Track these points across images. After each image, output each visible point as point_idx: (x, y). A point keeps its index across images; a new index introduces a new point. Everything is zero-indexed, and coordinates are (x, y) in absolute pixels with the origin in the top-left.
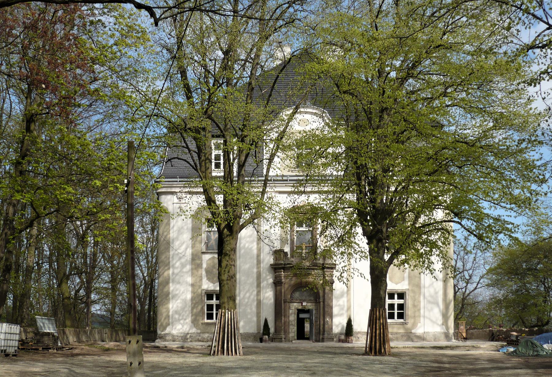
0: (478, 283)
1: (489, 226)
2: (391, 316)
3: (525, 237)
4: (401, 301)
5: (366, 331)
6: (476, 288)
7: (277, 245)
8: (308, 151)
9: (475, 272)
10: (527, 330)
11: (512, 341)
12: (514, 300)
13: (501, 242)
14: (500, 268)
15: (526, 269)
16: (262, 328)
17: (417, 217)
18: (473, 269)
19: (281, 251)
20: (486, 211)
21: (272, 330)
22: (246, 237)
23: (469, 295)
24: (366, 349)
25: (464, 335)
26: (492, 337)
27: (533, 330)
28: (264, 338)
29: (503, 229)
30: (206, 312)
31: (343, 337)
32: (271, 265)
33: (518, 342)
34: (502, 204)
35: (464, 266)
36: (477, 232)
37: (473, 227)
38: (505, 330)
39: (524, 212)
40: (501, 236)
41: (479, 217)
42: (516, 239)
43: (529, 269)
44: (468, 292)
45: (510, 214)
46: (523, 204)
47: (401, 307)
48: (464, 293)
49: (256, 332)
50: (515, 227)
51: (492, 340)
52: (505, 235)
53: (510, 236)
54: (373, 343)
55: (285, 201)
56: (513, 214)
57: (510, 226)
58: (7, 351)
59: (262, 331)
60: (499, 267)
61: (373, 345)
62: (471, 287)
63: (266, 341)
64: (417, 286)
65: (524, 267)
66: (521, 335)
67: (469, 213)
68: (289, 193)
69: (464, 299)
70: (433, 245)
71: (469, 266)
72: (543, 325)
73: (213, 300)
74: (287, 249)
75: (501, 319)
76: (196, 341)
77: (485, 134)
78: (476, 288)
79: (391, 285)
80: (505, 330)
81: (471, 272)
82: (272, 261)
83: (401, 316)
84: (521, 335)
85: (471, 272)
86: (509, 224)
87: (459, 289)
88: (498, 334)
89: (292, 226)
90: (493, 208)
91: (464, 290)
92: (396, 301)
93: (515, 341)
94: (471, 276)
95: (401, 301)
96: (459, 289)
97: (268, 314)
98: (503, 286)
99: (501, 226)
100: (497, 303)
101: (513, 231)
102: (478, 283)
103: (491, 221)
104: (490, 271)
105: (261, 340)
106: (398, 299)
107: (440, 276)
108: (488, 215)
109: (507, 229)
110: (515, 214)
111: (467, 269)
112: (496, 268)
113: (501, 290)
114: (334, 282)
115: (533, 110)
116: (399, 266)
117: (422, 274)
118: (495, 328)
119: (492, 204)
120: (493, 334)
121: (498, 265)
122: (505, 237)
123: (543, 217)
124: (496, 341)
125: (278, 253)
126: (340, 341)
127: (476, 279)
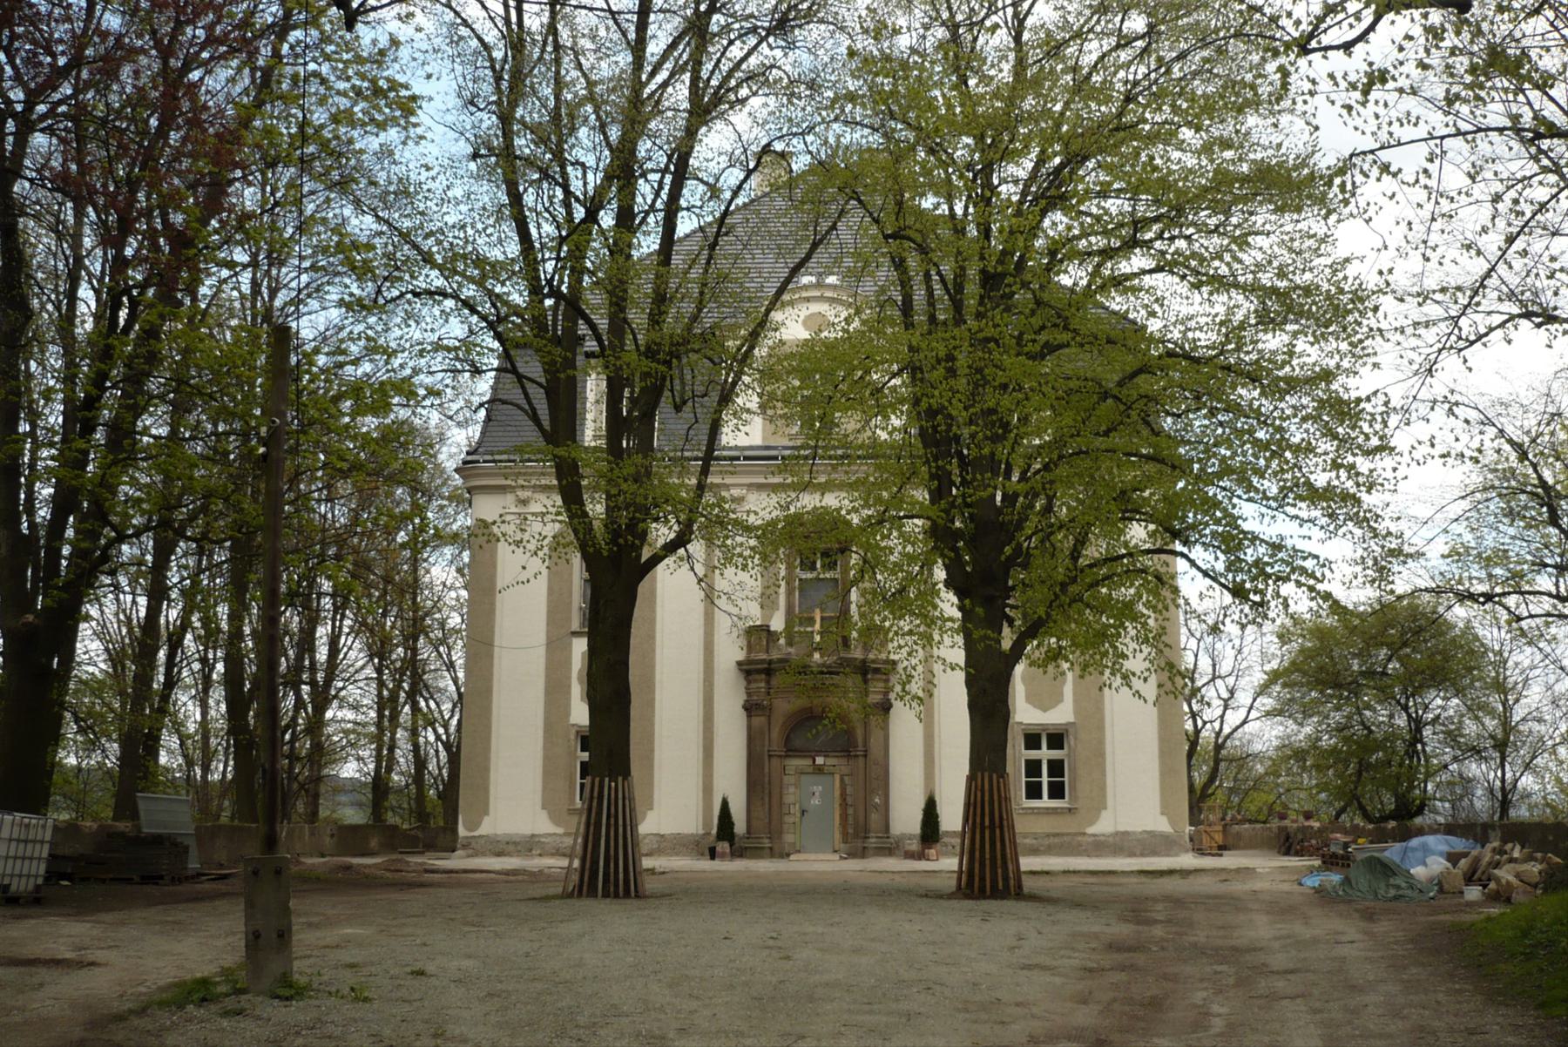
0: (1251, 708)
1: (1257, 563)
2: (1034, 791)
3: (1358, 595)
4: (1056, 754)
5: (960, 828)
6: (1245, 722)
7: (754, 613)
8: (822, 383)
9: (1243, 682)
10: (1371, 826)
11: (1334, 855)
12: (1334, 751)
13: (1290, 602)
14: (1298, 670)
15: (1362, 673)
16: (716, 821)
17: (1081, 542)
18: (1237, 672)
19: (765, 629)
20: (1246, 526)
21: (740, 827)
22: (672, 592)
23: (1228, 737)
24: (959, 879)
25: (1219, 838)
26: (1288, 844)
27: (1385, 829)
28: (719, 849)
29: (1293, 570)
30: (1066, 779)
31: (914, 846)
32: (739, 664)
33: (1348, 859)
34: (1289, 509)
35: (1214, 665)
36: (1230, 576)
37: (1220, 566)
38: (1317, 825)
39: (1344, 529)
40: (1287, 589)
41: (1232, 540)
42: (1327, 596)
43: (1369, 674)
44: (1227, 730)
45: (1307, 533)
46: (1337, 504)
47: (1056, 768)
48: (1218, 734)
49: (701, 832)
50: (1324, 566)
51: (1287, 853)
52: (1299, 584)
53: (1311, 589)
54: (977, 865)
55: (761, 508)
56: (1316, 533)
57: (1309, 564)
58: (13, 888)
59: (714, 831)
60: (1294, 666)
61: (977, 871)
62: (1233, 719)
63: (723, 856)
64: (1092, 713)
65: (1356, 668)
66: (1355, 842)
67: (1207, 531)
68: (774, 488)
69: (1219, 747)
70: (1127, 611)
71: (1225, 668)
72: (1412, 816)
73: (1039, 748)
74: (777, 623)
75: (1308, 796)
76: (553, 855)
77: (1233, 332)
78: (1245, 722)
79: (1024, 712)
80: (1317, 825)
81: (1231, 681)
82: (741, 655)
83: (1057, 791)
84: (1355, 842)
85: (1231, 681)
86: (1305, 558)
87: (1205, 723)
88: (1300, 837)
89: (790, 568)
90: (1267, 519)
91: (1217, 725)
92: (1045, 754)
93: (1343, 857)
94: (1232, 692)
95: (1056, 754)
96: (1205, 723)
97: (731, 783)
98: (1307, 714)
99: (1292, 564)
100: (1294, 754)
101: (1318, 575)
102: (1251, 708)
103: (1262, 550)
104: (1274, 677)
105: (713, 854)
106: (1049, 748)
107: (1150, 690)
108: (1254, 538)
109: (1303, 571)
110: (1322, 534)
111: (1223, 673)
112: (1286, 672)
113: (1301, 725)
114: (891, 706)
115: (1350, 281)
116: (1042, 664)
117: (1106, 690)
118: (1293, 822)
119: (1264, 510)
120: (1287, 839)
121: (1293, 663)
122: (1300, 591)
123: (1393, 544)
124: (1297, 854)
125: (758, 635)
126: (910, 855)
127: (1244, 698)
